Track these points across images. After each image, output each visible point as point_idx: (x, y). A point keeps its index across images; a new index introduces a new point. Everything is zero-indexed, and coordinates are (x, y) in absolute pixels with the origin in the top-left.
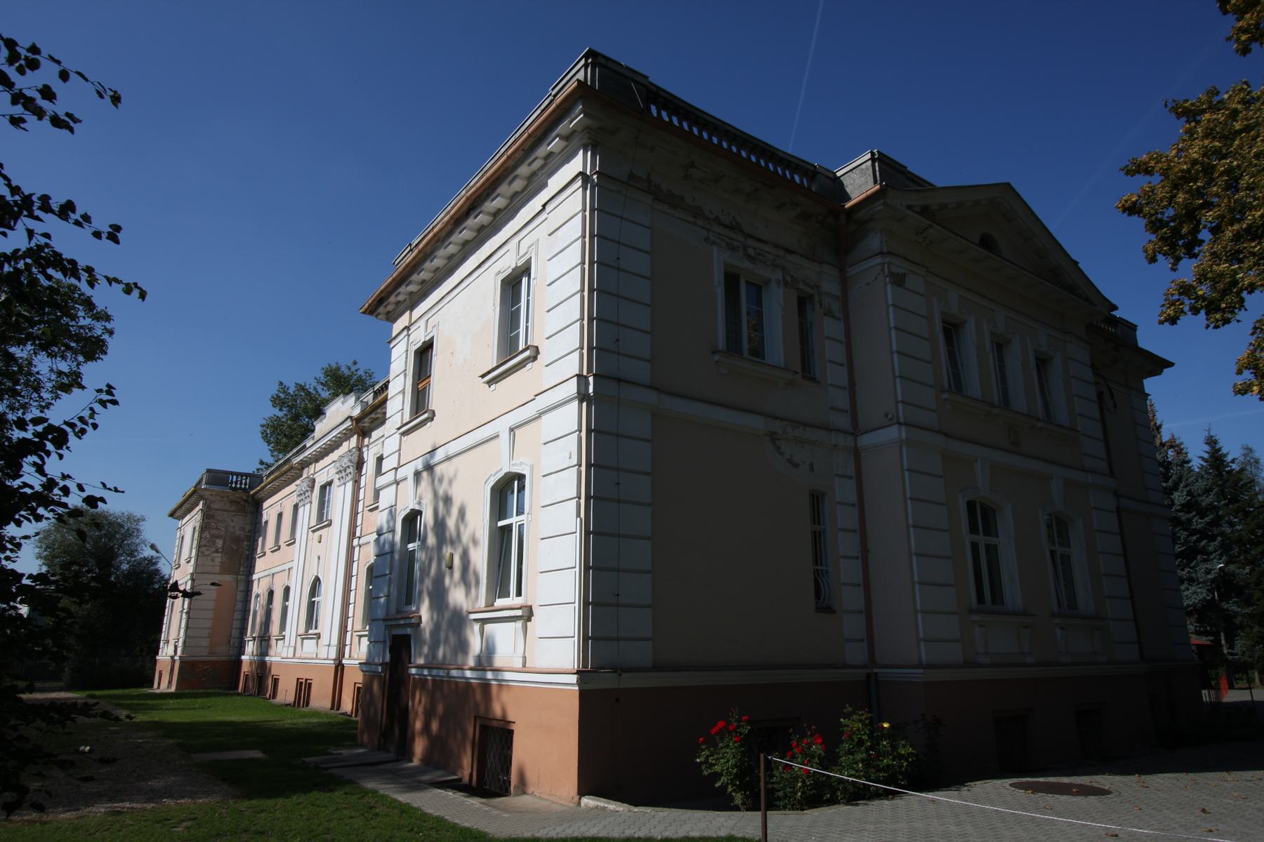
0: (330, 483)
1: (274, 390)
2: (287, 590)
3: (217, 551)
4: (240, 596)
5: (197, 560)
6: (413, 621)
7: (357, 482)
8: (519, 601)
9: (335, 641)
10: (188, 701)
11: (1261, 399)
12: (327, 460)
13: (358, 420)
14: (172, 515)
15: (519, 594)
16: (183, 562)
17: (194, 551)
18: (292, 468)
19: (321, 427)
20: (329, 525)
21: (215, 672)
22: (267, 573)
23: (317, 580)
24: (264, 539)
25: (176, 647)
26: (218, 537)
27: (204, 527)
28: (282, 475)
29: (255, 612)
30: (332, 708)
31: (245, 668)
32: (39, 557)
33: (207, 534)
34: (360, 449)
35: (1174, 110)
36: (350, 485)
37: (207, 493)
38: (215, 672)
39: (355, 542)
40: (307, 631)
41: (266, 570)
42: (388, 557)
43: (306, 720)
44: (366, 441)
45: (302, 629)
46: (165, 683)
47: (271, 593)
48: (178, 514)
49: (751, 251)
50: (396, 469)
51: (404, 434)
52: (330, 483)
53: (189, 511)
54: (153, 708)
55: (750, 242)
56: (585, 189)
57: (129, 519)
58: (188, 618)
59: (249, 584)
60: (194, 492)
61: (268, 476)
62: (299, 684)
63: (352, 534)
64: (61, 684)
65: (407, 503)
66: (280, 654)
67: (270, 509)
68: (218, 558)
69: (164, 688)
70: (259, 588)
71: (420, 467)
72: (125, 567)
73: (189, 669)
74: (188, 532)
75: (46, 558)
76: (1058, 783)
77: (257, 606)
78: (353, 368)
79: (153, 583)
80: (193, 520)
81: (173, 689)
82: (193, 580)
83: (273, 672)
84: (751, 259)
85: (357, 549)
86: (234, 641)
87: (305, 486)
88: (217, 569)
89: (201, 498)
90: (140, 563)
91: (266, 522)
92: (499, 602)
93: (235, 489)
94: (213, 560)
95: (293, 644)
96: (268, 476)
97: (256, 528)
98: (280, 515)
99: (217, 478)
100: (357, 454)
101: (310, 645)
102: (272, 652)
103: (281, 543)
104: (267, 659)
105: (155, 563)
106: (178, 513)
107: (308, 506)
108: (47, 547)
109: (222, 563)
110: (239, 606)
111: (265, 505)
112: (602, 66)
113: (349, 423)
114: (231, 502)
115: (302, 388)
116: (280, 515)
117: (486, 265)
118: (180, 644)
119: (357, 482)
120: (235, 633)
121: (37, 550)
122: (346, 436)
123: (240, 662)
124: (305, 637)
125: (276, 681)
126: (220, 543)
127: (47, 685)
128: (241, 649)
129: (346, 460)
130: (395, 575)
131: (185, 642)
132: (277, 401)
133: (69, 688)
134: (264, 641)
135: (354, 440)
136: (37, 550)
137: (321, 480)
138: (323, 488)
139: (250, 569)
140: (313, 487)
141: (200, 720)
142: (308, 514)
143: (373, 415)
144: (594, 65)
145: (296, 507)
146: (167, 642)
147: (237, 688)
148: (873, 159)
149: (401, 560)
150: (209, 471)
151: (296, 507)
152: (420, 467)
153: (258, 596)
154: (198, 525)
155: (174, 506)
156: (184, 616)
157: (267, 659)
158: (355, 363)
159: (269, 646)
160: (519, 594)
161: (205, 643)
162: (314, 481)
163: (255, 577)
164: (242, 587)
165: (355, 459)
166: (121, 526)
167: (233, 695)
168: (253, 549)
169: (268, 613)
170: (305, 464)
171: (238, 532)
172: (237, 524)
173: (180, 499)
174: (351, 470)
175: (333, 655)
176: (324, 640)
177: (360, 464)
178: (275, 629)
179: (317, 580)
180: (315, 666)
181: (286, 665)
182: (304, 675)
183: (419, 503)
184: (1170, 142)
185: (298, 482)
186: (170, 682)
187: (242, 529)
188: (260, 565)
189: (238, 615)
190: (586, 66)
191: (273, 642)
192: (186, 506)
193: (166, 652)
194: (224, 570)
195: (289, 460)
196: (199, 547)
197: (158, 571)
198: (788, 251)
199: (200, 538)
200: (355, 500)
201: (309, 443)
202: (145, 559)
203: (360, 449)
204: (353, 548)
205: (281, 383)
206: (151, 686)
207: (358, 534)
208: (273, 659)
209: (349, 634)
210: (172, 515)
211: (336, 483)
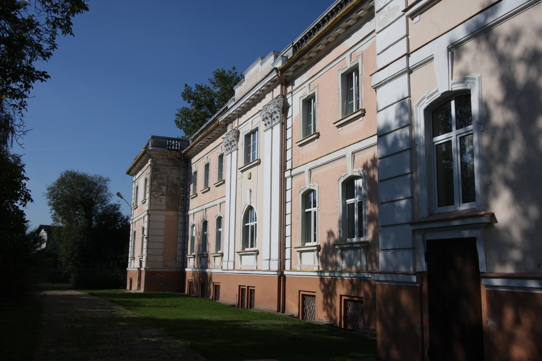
0: (254, 132)
1: (183, 89)
2: (219, 220)
3: (163, 195)
4: (180, 226)
5: (150, 201)
6: (485, 220)
7: (284, 124)
8: (315, 244)
9: (275, 255)
10: (159, 300)
12: (254, 110)
13: (282, 70)
14: (128, 173)
15: (315, 241)
16: (139, 203)
17: (148, 196)
18: (218, 125)
19: (239, 91)
20: (259, 163)
21: (167, 279)
22: (200, 209)
23: (250, 208)
24: (195, 184)
25: (141, 262)
26: (163, 184)
27: (153, 177)
28: (208, 134)
29: (193, 238)
30: (279, 310)
31: (189, 277)
32: (50, 204)
33: (155, 182)
34: (284, 96)
36: (277, 129)
37: (153, 152)
38: (167, 279)
39: (287, 174)
40: (243, 249)
41: (198, 207)
42: (407, 154)
43: (266, 322)
44: (289, 89)
45: (239, 247)
46: (135, 286)
47: (205, 223)
48: (133, 171)
50: (408, 55)
51: (413, 16)
52: (254, 132)
53: (140, 168)
54: (138, 305)
57: (100, 179)
58: (148, 242)
59: (186, 217)
60: (145, 152)
61: (193, 140)
62: (242, 290)
63: (283, 168)
64: (70, 285)
65: (439, 80)
66: (215, 267)
67: (197, 164)
68: (164, 199)
69: (134, 289)
70: (195, 220)
71: (460, 33)
72: (100, 211)
73: (152, 276)
74: (141, 183)
75: (54, 205)
76: (63, 295)
77: (194, 232)
78: (233, 72)
79: (117, 222)
80: (145, 172)
81: (142, 290)
82: (149, 215)
83: (213, 281)
85: (289, 181)
86: (179, 258)
87: (231, 137)
88: (164, 207)
89: (150, 157)
90: (109, 209)
91: (196, 173)
92: (307, 244)
93: (171, 150)
94: (161, 201)
95: (232, 259)
96: (193, 140)
97: (188, 178)
98: (207, 166)
99: (159, 142)
100: (282, 100)
101: (248, 262)
102: (211, 265)
103: (211, 185)
104: (208, 270)
105: (117, 209)
106: (132, 171)
107: (234, 153)
108: (54, 198)
109: (167, 203)
110: (180, 233)
111: (193, 160)
113: (274, 74)
114: (170, 159)
115: (200, 87)
116: (207, 166)
118: (144, 259)
119: (284, 124)
120: (179, 253)
121: (48, 200)
122: (270, 88)
123: (184, 273)
124: (242, 254)
125: (217, 288)
126: (164, 189)
127: (61, 285)
128: (184, 264)
129: (272, 107)
130: (420, 171)
131: (147, 258)
132: (188, 95)
133: (76, 288)
134: (203, 257)
135: (277, 91)
136: (48, 200)
137: (244, 130)
138: (248, 136)
139: (186, 207)
140: (238, 137)
141: (178, 317)
142: (234, 160)
143: (298, 63)
145: (221, 157)
146: (134, 258)
147: (184, 290)
149: (428, 156)
150: (153, 137)
151: (221, 157)
152: (460, 33)
153: (193, 226)
154: (149, 177)
155: (130, 165)
156: (145, 240)
157: (208, 270)
158: (234, 69)
159: (207, 261)
160: (315, 241)
161: (160, 259)
162: (238, 132)
163: (190, 212)
164: (181, 220)
165: (281, 105)
166: (96, 184)
167: (179, 296)
168: (187, 193)
169: (204, 238)
170: (230, 120)
171: (176, 181)
172: (174, 175)
173: (133, 162)
174: (278, 114)
175: (275, 266)
176: (264, 254)
177: (285, 109)
178: (211, 248)
179: (250, 208)
180: (257, 276)
181: (228, 275)
182: (246, 283)
183: (464, 79)
185: (224, 136)
186: (139, 286)
187: (178, 179)
188: (193, 204)
189: (180, 240)
191: (211, 258)
192: (139, 164)
193: (133, 266)
194: (169, 208)
195: (215, 119)
196: (151, 192)
197: (119, 214)
199: (151, 185)
201: (230, 104)
202: (111, 206)
203: (284, 96)
204: (285, 179)
205: (186, 85)
206: (125, 287)
207: (289, 166)
208: (213, 271)
209: (288, 251)
210: (128, 173)
211: (262, 128)
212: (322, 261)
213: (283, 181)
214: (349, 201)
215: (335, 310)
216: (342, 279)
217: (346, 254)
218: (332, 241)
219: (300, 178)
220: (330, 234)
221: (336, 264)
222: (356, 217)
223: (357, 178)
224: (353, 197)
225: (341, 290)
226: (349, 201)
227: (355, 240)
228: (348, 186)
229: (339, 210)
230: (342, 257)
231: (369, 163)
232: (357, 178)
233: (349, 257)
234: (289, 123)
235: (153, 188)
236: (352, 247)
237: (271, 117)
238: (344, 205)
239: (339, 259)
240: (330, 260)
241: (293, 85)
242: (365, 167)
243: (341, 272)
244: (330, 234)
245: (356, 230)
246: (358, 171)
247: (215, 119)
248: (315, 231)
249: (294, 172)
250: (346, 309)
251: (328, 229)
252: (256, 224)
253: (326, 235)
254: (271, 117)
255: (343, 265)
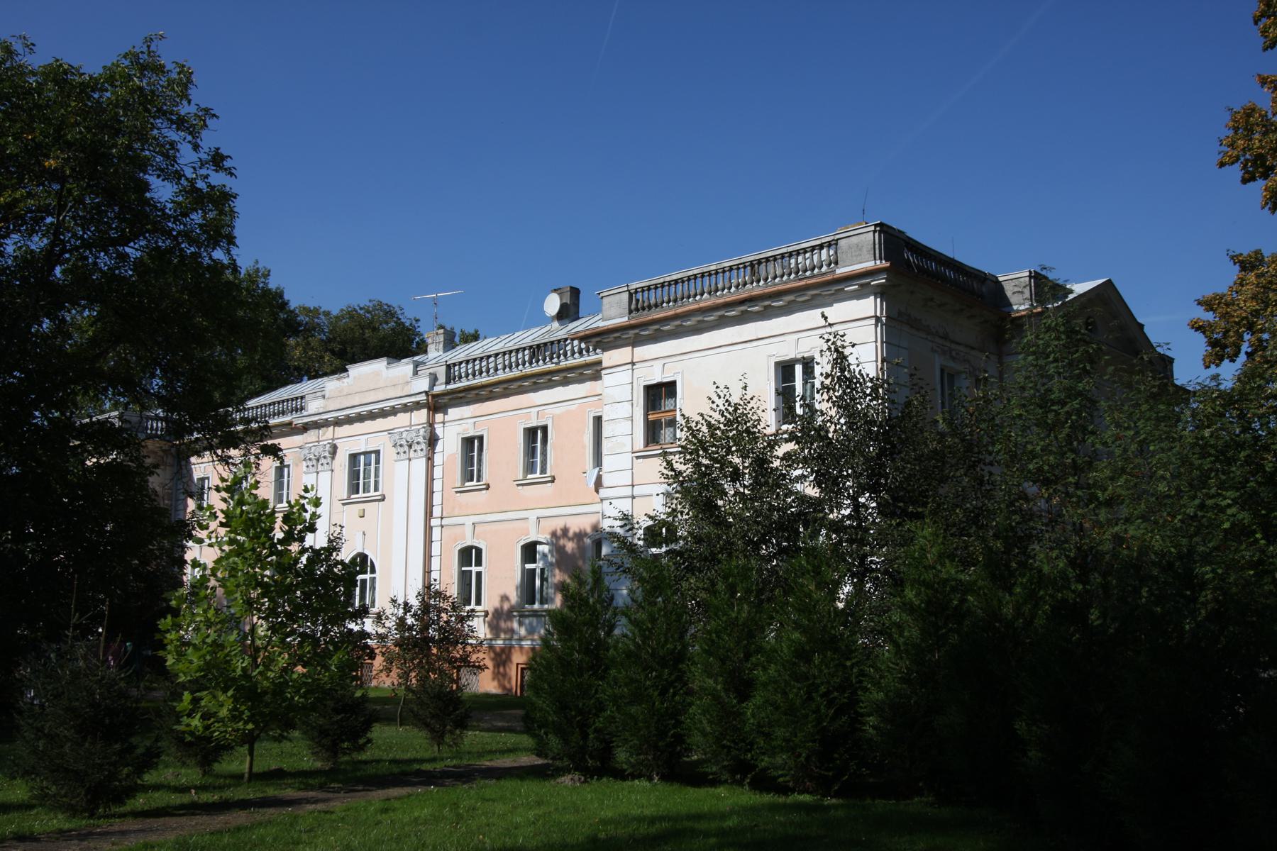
7: (430, 460)
11: (1273, 210)
35: (1232, 258)
36: (420, 465)
49: (954, 353)
55: (953, 346)
56: (876, 326)
84: (953, 359)
112: (885, 233)
117: (755, 344)
119: (430, 460)
122: (417, 406)
144: (880, 232)
148: (1030, 277)
174: (423, 446)
177: (432, 441)
184: (1223, 279)
190: (874, 232)
198: (973, 348)
200: (430, 479)
203: (431, 425)
204: (431, 528)
211: (388, 454)
212: (490, 626)
213: (428, 530)
214: (529, 566)
215: (510, 679)
216: (521, 647)
217: (527, 621)
218: (506, 606)
219: (458, 530)
220: (505, 598)
221: (512, 631)
222: (538, 582)
223: (541, 543)
224: (535, 562)
225: (519, 658)
226: (529, 566)
227: (536, 606)
228: (529, 551)
229: (517, 577)
230: (520, 624)
231: (559, 532)
232: (541, 543)
233: (531, 624)
234: (438, 459)
235: (258, 384)
236: (535, 614)
237: (410, 446)
238: (523, 569)
239: (515, 625)
240: (503, 625)
241: (446, 413)
242: (554, 534)
243: (521, 639)
244: (505, 598)
245: (538, 596)
246: (544, 536)
247: (202, 788)
248: (377, 475)
249: (445, 522)
250: (522, 677)
251: (502, 592)
252: (373, 580)
253: (498, 599)
254: (410, 446)
255: (523, 632)
